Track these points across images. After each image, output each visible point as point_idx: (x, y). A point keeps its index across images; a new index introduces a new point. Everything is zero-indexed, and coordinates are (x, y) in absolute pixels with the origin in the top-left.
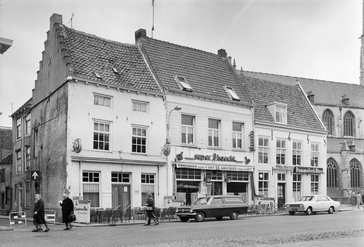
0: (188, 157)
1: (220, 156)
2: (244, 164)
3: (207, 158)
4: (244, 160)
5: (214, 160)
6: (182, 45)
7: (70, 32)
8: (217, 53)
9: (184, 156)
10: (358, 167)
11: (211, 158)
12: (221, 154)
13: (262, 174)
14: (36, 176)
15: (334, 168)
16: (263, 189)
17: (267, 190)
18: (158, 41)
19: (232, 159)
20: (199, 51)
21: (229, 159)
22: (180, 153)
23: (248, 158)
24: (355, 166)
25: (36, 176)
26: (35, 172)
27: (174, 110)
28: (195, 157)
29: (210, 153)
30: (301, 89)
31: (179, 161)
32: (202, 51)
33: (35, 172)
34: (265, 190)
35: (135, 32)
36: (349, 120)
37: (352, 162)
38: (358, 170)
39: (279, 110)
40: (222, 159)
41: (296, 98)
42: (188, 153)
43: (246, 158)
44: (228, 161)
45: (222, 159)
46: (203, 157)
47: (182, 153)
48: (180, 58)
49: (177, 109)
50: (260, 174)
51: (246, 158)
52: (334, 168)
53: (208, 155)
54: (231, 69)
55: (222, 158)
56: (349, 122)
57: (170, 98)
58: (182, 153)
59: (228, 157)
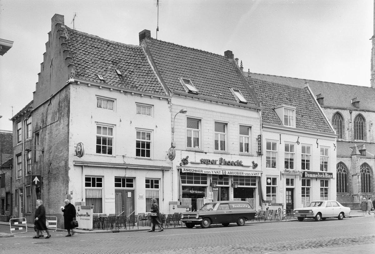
0: (193, 161)
1: (227, 160)
2: (251, 169)
3: (213, 163)
4: (252, 165)
5: (220, 164)
6: (188, 46)
7: (73, 33)
8: (223, 55)
9: (189, 160)
10: (368, 172)
11: (218, 163)
12: (227, 158)
13: (270, 178)
14: (37, 181)
15: (344, 173)
16: (271, 194)
17: (275, 196)
18: (163, 42)
19: (239, 164)
20: (205, 52)
21: (236, 163)
22: (185, 158)
23: (255, 163)
24: (365, 171)
25: (37, 181)
26: (36, 177)
27: (180, 113)
28: (201, 161)
29: (217, 158)
30: (310, 92)
31: (184, 166)
32: (208, 52)
33: (36, 177)
34: (273, 196)
35: (139, 33)
36: (360, 123)
37: (363, 166)
38: (369, 175)
39: (287, 113)
40: (228, 164)
41: (305, 101)
42: (194, 158)
43: (253, 163)
44: (235, 165)
45: (228, 164)
46: (209, 161)
47: (188, 157)
48: (186, 60)
49: (182, 112)
50: (267, 178)
51: (253, 163)
52: (344, 173)
53: (215, 159)
54: (238, 71)
55: (229, 162)
56: (360, 126)
57: (175, 101)
58: (188, 157)
59: (234, 161)
